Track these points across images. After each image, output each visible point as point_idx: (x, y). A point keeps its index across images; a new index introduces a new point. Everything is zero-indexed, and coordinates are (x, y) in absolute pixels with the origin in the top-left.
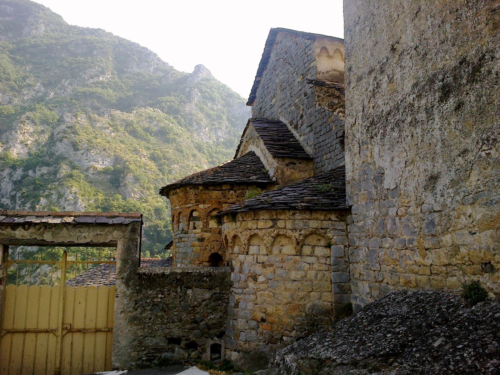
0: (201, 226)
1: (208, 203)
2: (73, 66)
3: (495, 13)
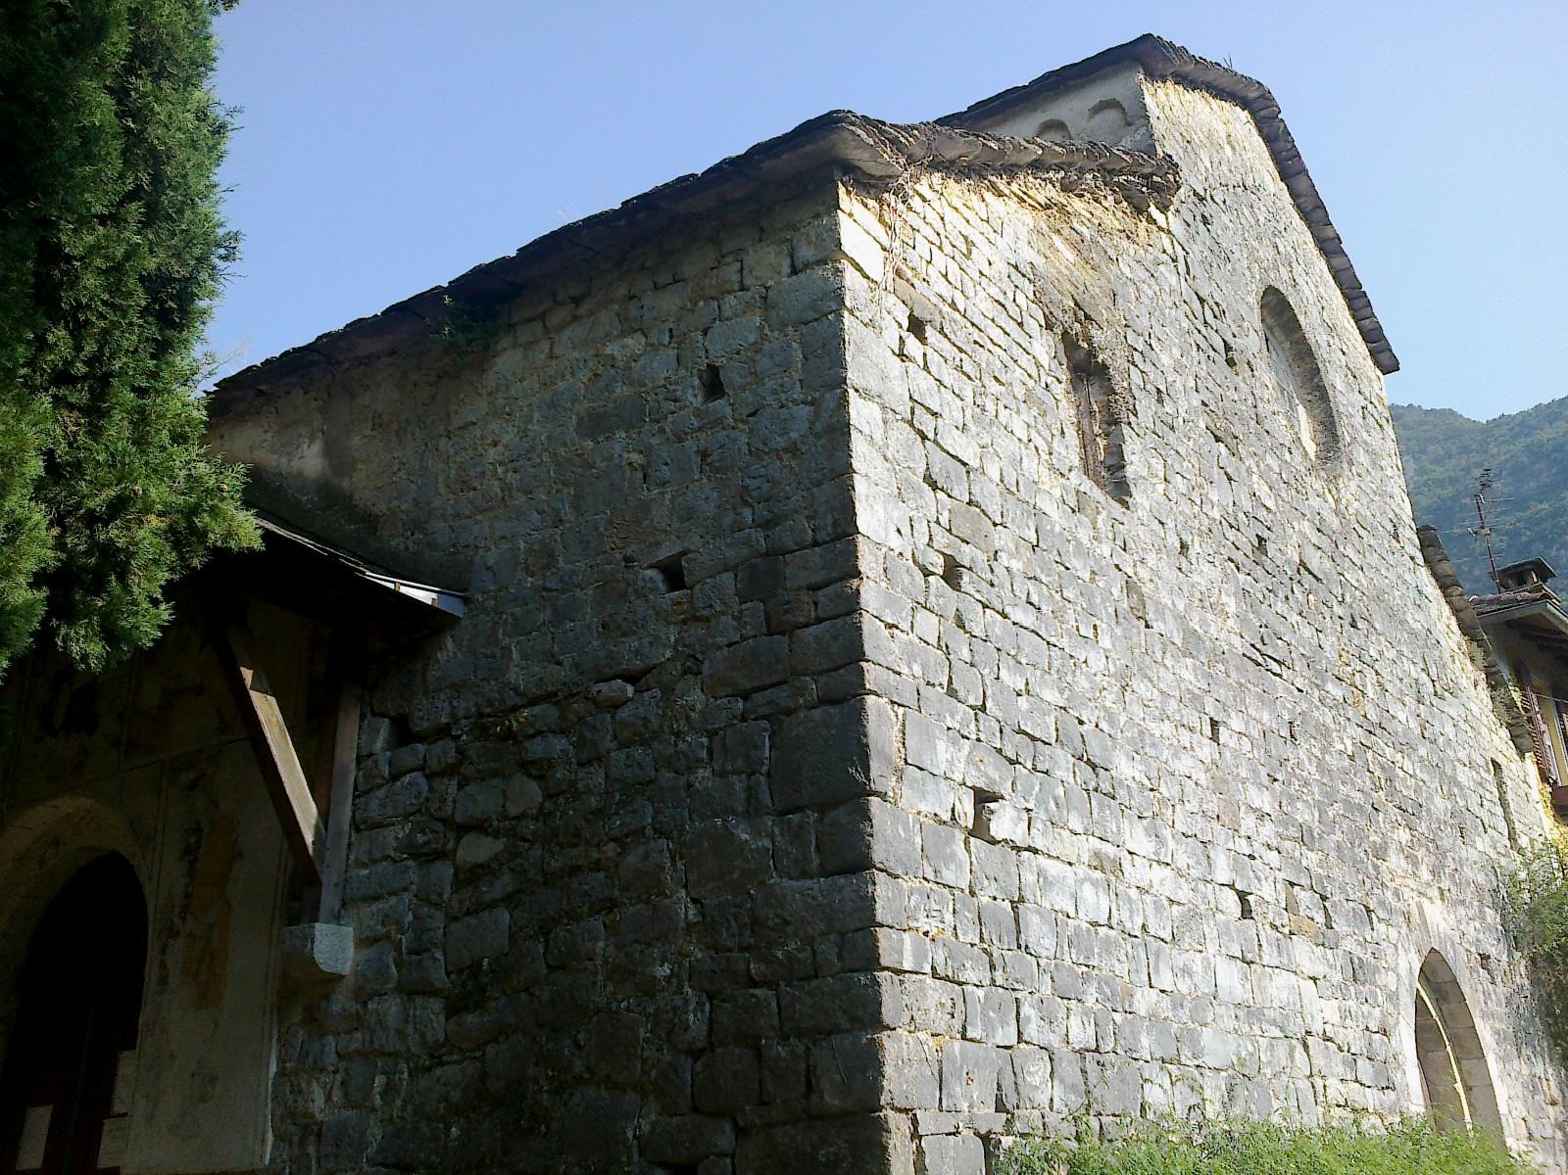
2: (1524, 539)
3: (576, 318)
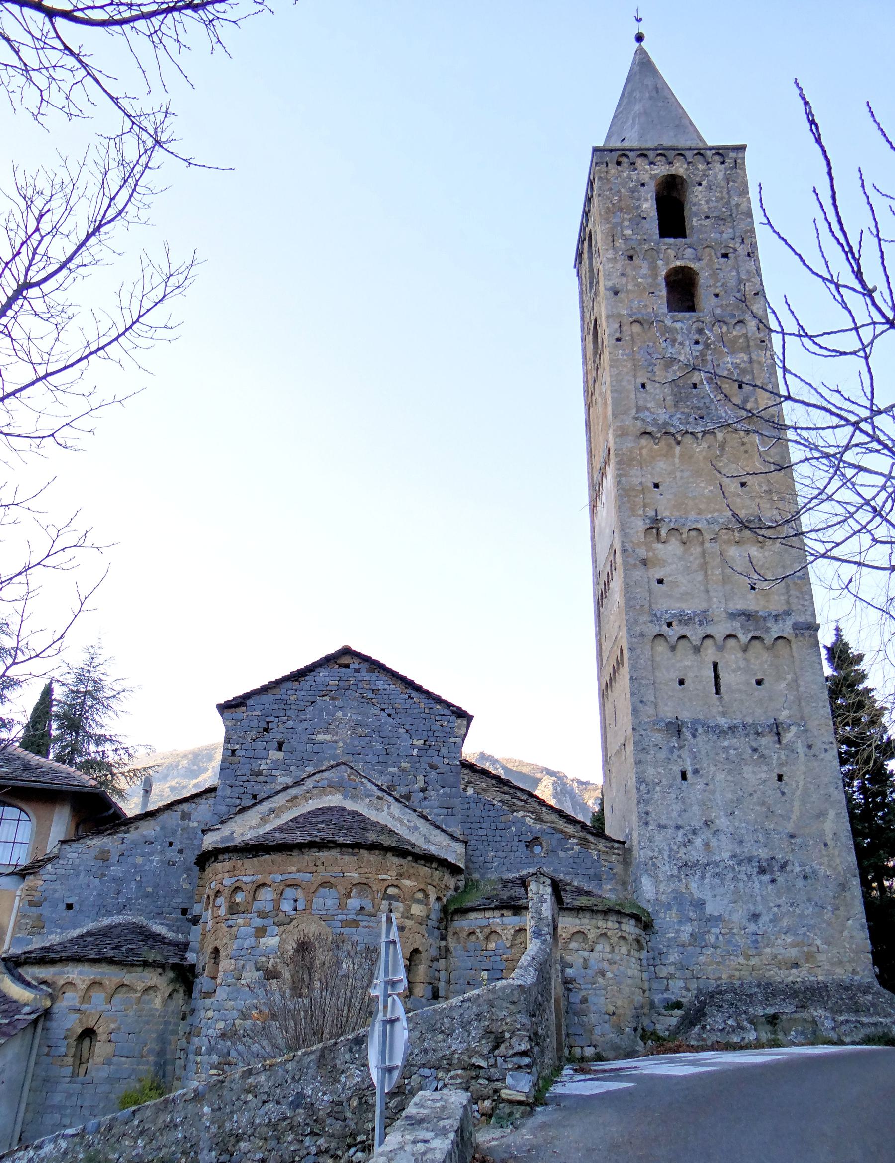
0: (401, 909)
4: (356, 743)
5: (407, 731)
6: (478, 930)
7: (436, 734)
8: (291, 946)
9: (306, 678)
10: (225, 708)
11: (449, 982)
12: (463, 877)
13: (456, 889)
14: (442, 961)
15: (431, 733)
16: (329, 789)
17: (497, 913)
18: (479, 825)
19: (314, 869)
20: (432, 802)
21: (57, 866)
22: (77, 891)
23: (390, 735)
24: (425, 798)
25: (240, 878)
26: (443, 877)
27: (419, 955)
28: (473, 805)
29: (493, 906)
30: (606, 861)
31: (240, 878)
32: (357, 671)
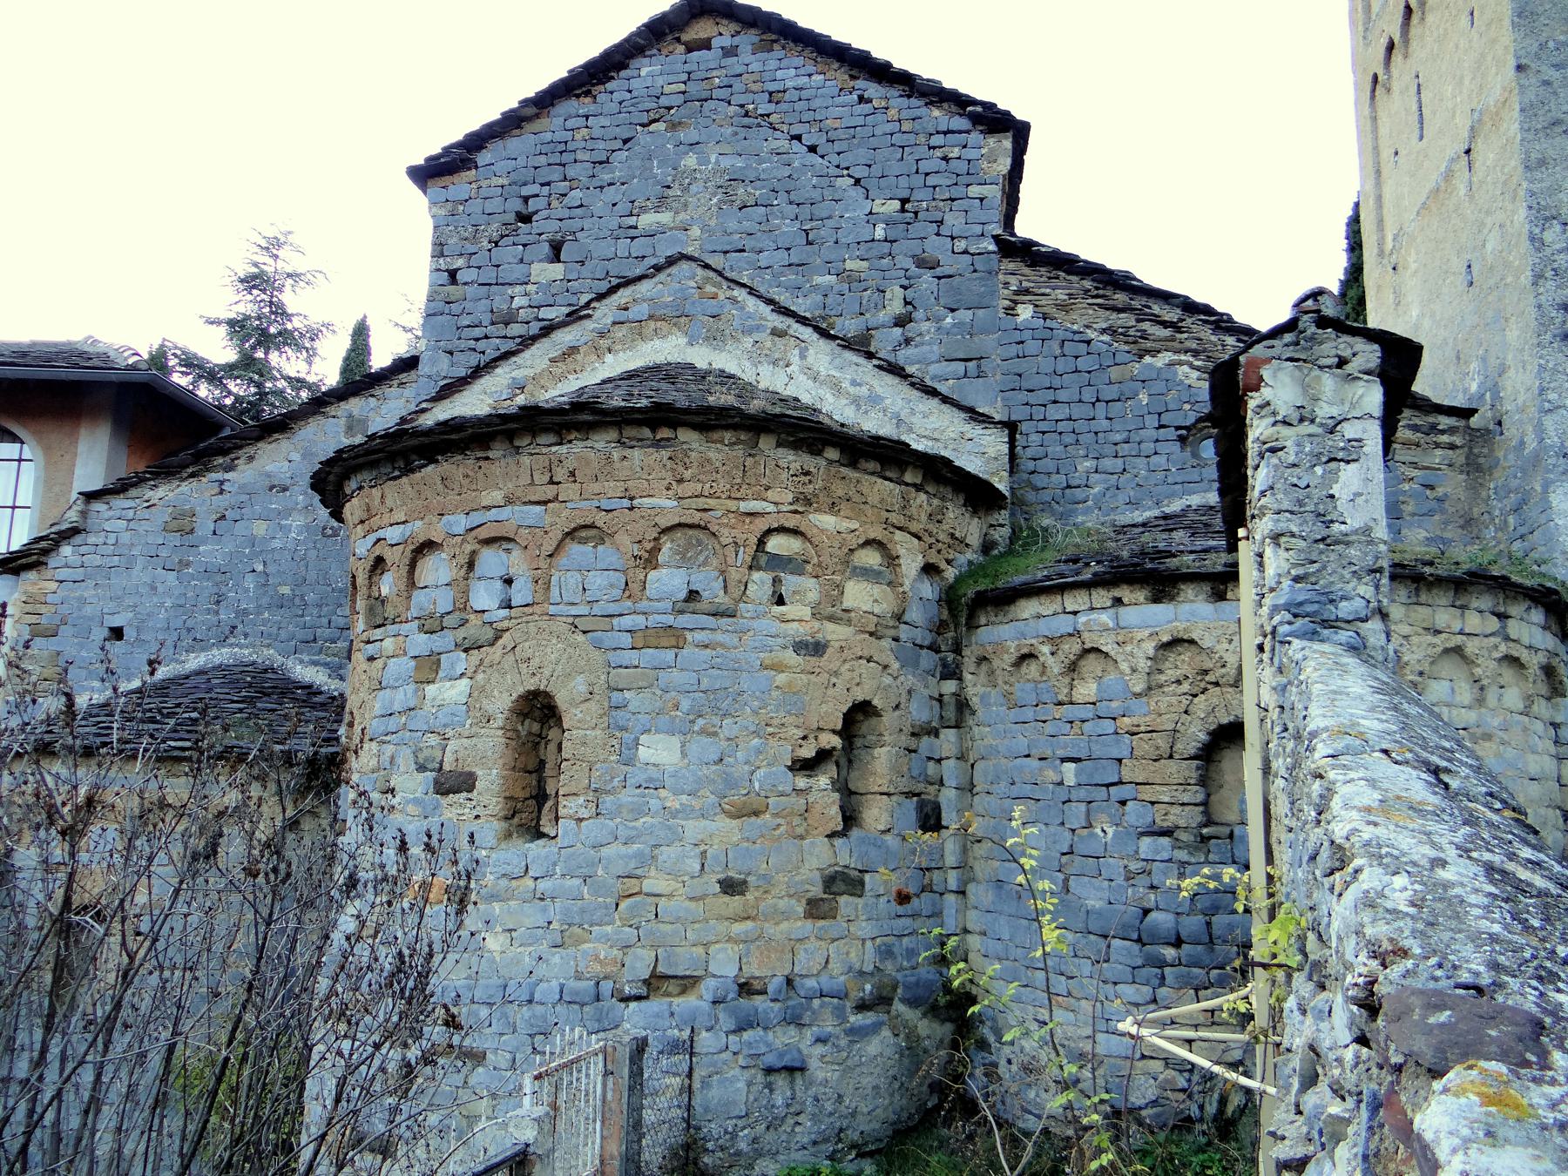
0: (813, 596)
1: (850, 514)
4: (732, 225)
5: (857, 182)
6: (1046, 649)
7: (931, 180)
8: (501, 703)
9: (610, 86)
10: (429, 173)
11: (969, 788)
12: (1003, 516)
13: (987, 547)
14: (949, 735)
15: (918, 180)
16: (652, 324)
17: (1102, 597)
18: (1050, 395)
19: (550, 491)
20: (926, 348)
21: (83, 549)
22: (129, 601)
23: (816, 194)
24: (908, 341)
25: (381, 534)
26: (942, 511)
27: (874, 721)
28: (1032, 346)
29: (1087, 575)
30: (1414, 465)
31: (381, 534)
32: (730, 52)
